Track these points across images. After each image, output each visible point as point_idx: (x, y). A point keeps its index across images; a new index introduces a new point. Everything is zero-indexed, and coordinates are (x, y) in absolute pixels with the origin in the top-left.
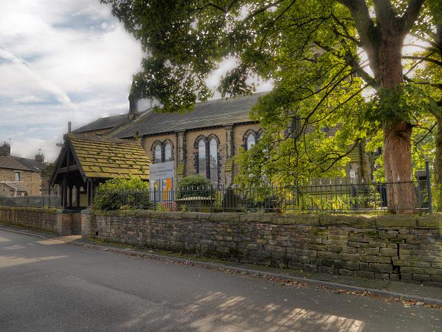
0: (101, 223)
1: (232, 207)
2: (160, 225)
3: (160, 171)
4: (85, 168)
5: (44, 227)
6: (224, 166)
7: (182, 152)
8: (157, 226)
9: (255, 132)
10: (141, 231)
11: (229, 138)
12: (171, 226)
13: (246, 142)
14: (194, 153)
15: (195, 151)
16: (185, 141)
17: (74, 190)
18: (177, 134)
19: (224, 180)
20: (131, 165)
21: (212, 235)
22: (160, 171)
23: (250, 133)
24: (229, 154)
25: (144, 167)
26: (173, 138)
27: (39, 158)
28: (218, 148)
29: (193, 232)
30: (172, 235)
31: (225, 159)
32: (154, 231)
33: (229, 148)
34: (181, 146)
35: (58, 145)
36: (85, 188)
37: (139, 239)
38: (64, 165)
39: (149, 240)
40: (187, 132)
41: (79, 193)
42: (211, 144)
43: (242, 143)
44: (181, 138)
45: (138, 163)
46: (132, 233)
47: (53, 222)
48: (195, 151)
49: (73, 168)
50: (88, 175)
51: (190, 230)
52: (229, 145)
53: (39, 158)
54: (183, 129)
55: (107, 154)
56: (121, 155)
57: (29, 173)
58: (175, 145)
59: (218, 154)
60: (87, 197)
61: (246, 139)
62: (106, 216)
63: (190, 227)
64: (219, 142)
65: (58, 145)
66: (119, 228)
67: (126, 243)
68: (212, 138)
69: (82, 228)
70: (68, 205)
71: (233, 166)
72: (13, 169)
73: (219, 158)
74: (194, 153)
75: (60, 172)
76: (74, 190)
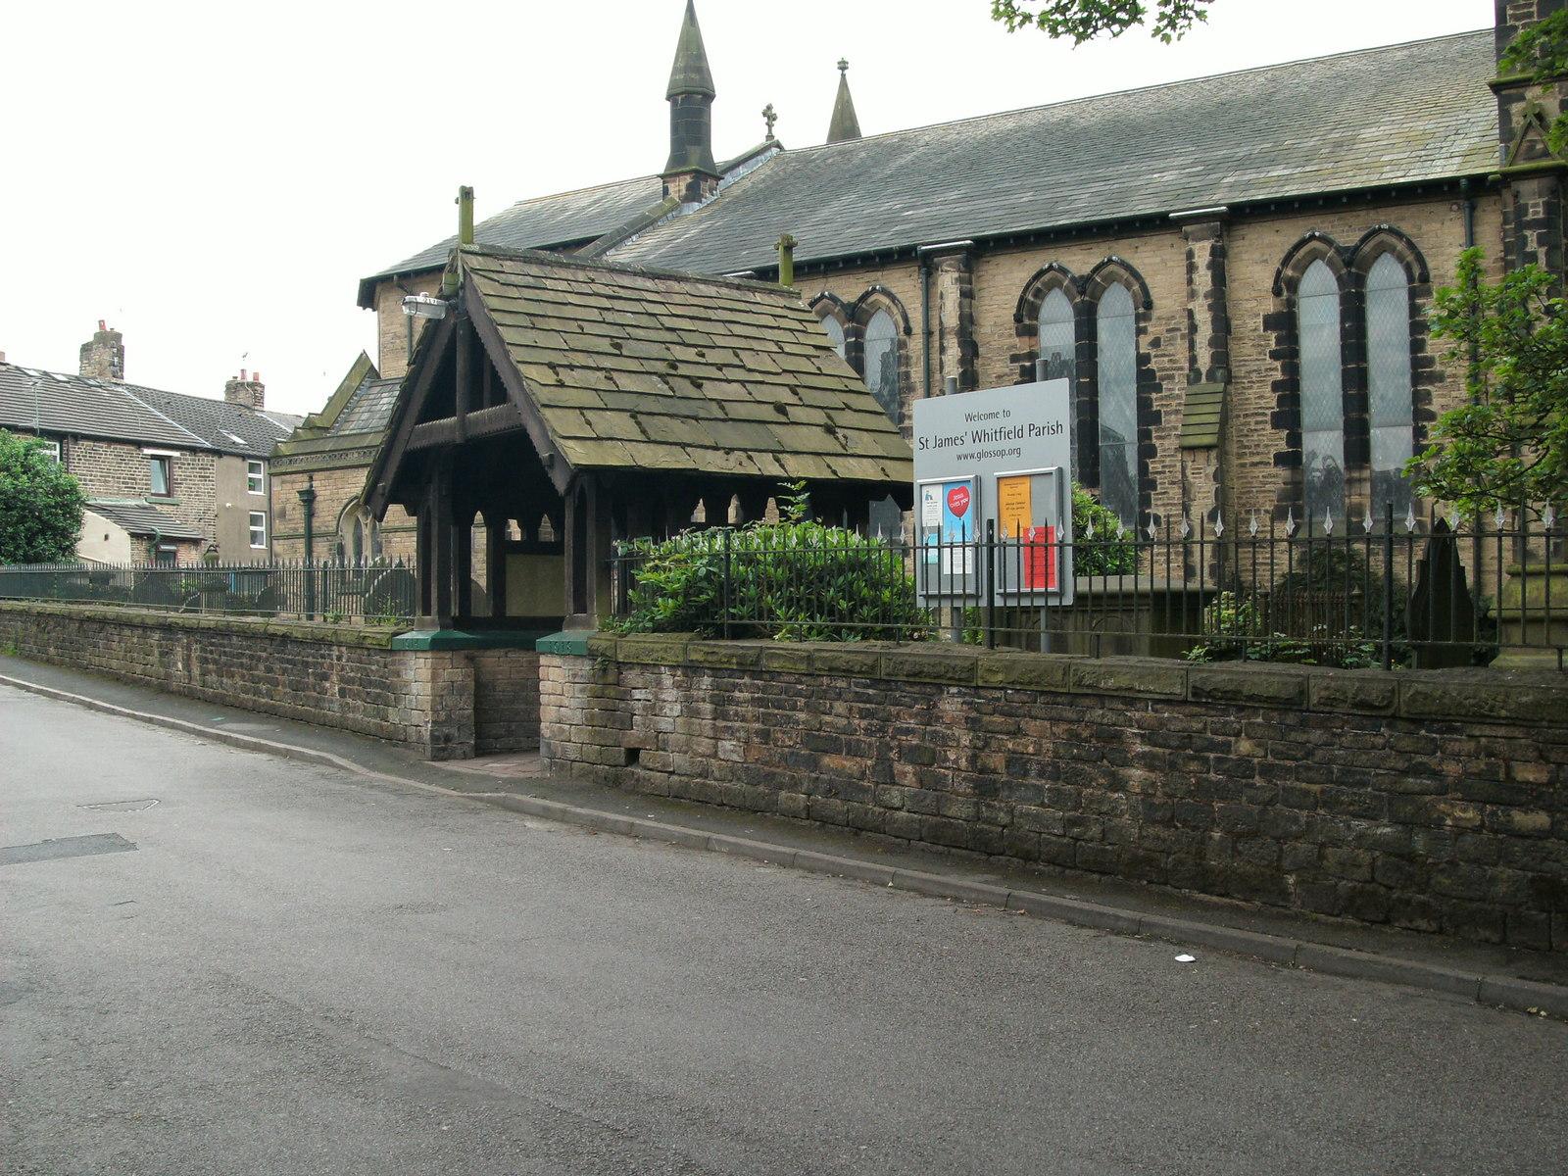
0: (653, 708)
1: (1441, 633)
2: (1032, 726)
3: (977, 437)
4: (562, 423)
5: (333, 710)
6: (1170, 421)
7: (953, 351)
8: (1016, 733)
9: (1340, 251)
10: (910, 754)
11: (1204, 279)
12: (1117, 737)
13: (1291, 304)
14: (1014, 359)
15: (1022, 345)
16: (967, 295)
17: (480, 537)
18: (921, 260)
19: (1175, 492)
20: (781, 408)
21: (1407, 793)
22: (977, 437)
23: (1314, 256)
24: (1204, 360)
25: (845, 418)
26: (904, 284)
27: (246, 392)
28: (1140, 331)
29: (1267, 771)
30: (1118, 784)
31: (1178, 387)
32: (997, 761)
33: (1205, 332)
34: (951, 318)
35: (106, 347)
36: (558, 525)
37: (894, 796)
38: (438, 403)
39: (959, 811)
40: (982, 250)
41: (499, 546)
42: (1101, 311)
43: (1270, 306)
44: (948, 282)
45: (809, 396)
46: (850, 765)
47: (387, 692)
48: (1022, 345)
49: (487, 418)
50: (578, 454)
51: (1244, 761)
52: (1204, 317)
53: (246, 392)
54: (962, 235)
55: (656, 350)
56: (727, 357)
57: (206, 459)
58: (917, 326)
59: (1142, 360)
60: (568, 570)
61: (1293, 285)
62: (692, 669)
63: (1245, 746)
64: (1419, 283)
65: (106, 347)
66: (765, 736)
67: (809, 812)
68: (1110, 279)
69: (545, 729)
70: (454, 611)
71: (1224, 422)
72: (139, 444)
73: (1147, 379)
74: (1014, 359)
75: (418, 444)
76: (480, 537)
